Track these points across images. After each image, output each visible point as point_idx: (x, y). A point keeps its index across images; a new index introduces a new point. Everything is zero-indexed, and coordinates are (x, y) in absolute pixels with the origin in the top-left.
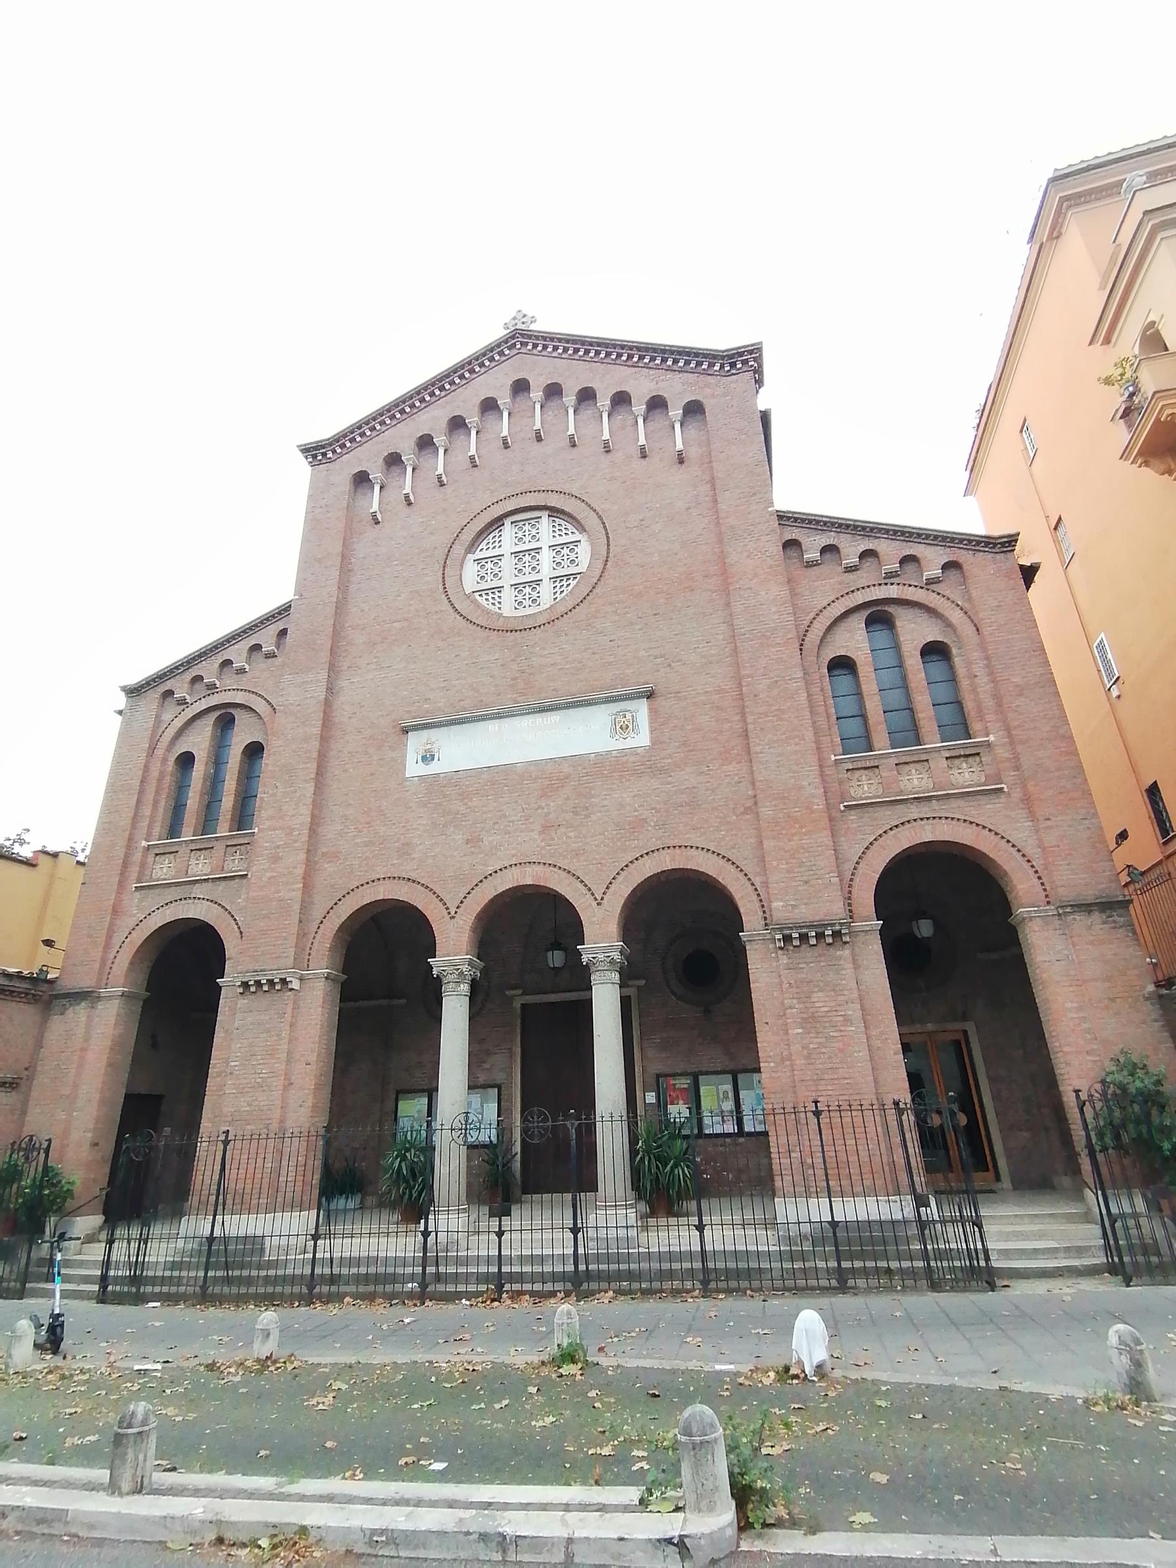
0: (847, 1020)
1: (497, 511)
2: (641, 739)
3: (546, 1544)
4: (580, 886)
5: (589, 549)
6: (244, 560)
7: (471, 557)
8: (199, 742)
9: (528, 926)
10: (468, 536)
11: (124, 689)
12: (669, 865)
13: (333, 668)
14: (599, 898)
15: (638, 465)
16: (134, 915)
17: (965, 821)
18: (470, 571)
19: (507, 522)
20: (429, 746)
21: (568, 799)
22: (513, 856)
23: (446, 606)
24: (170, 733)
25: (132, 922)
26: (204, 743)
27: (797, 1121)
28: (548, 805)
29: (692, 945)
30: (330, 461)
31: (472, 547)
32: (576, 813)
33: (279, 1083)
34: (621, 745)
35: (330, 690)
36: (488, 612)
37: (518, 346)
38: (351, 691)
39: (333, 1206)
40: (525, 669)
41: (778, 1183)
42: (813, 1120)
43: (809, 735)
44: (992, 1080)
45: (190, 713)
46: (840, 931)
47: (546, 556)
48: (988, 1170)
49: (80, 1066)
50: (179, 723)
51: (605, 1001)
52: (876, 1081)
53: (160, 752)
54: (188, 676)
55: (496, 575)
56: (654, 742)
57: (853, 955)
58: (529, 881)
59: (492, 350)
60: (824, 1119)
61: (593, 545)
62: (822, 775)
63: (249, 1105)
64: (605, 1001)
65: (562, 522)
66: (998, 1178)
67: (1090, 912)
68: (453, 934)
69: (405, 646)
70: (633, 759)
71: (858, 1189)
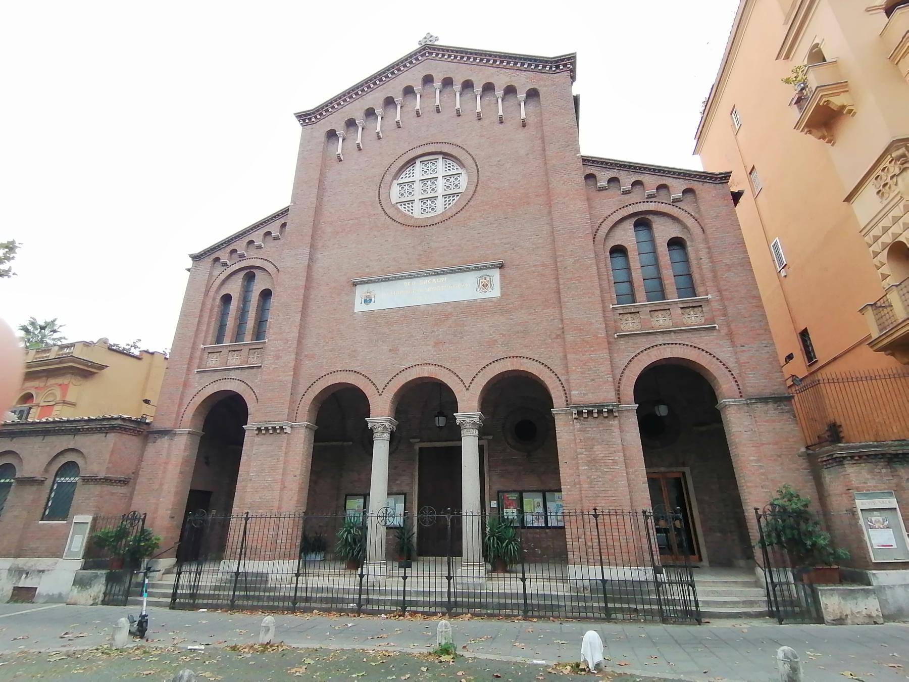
0: (615, 462)
6: (260, 181)
8: (234, 288)
9: (425, 401)
19: (418, 161)
25: (195, 391)
29: (522, 415)
31: (396, 176)
42: (593, 520)
45: (229, 271)
50: (222, 277)
51: (470, 446)
54: (229, 249)
56: (503, 294)
61: (469, 176)
63: (260, 498)
64: (470, 446)
66: (701, 559)
70: (490, 304)
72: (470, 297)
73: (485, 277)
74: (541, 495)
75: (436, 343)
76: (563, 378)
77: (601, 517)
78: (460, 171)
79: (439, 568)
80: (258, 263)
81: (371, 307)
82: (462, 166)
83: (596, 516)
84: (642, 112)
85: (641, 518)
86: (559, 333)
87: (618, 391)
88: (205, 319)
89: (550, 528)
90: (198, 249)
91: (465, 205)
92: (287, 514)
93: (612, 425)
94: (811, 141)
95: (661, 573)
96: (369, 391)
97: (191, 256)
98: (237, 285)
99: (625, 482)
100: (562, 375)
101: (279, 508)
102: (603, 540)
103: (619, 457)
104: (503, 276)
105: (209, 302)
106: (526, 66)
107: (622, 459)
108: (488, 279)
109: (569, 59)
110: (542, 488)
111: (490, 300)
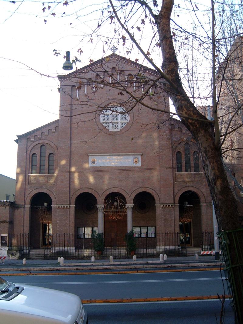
0: (172, 220)
2: (139, 164)
3: (183, 95)
6: (44, 108)
8: (37, 151)
9: (114, 198)
11: (17, 136)
12: (143, 191)
14: (130, 195)
17: (195, 187)
20: (94, 160)
22: (112, 186)
24: (30, 149)
25: (29, 192)
26: (36, 148)
30: (65, 81)
32: (125, 178)
34: (135, 165)
35: (71, 144)
40: (114, 143)
42: (64, 236)
44: (194, 229)
45: (34, 144)
46: (214, 164)
48: (190, 244)
50: (32, 146)
52: (175, 230)
53: (28, 153)
54: (33, 135)
55: (107, 119)
56: (141, 165)
60: (65, 236)
63: (62, 229)
64: (130, 214)
66: (191, 245)
67: (59, 269)
69: (87, 135)
71: (170, 245)
72: (131, 165)
73: (136, 158)
74: (147, 227)
75: (36, 165)
79: (71, 251)
81: (95, 165)
83: (166, 234)
85: (176, 234)
86: (159, 180)
88: (28, 164)
89: (141, 237)
93: (172, 210)
94: (55, 13)
97: (17, 136)
99: (174, 225)
100: (159, 194)
102: (65, 242)
104: (142, 159)
105: (28, 156)
106: (132, 65)
108: (137, 159)
110: (147, 225)
111: (137, 167)
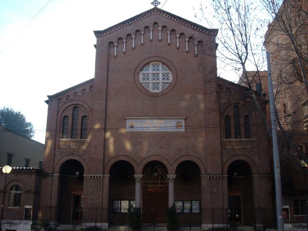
1: (149, 60)
4: (167, 162)
5: (172, 76)
6: (81, 68)
7: (141, 72)
8: (69, 113)
9: (154, 167)
10: (140, 67)
13: (106, 100)
15: (185, 54)
16: (59, 157)
18: (141, 76)
19: (151, 63)
20: (132, 124)
21: (165, 142)
23: (135, 86)
24: (62, 110)
27: (92, 210)
28: (161, 142)
29: (188, 172)
31: (141, 70)
33: (101, 198)
34: (178, 130)
36: (145, 89)
37: (156, 12)
38: (111, 106)
39: (77, 226)
40: (155, 105)
41: (203, 221)
42: (95, 210)
43: (219, 134)
45: (66, 105)
47: (161, 76)
49: (52, 191)
50: (64, 108)
51: (171, 186)
55: (148, 79)
57: (222, 181)
58: (156, 160)
59: (148, 12)
61: (172, 73)
62: (221, 143)
64: (171, 186)
65: (165, 67)
66: (241, 223)
68: (139, 170)
70: (181, 134)
76: (205, 164)
77: (98, 209)
78: (169, 72)
80: (80, 103)
82: (170, 70)
83: (96, 209)
84: (242, 54)
87: (222, 170)
90: (52, 94)
91: (170, 89)
92: (216, 208)
95: (228, 224)
96: (134, 164)
98: (65, 108)
101: (102, 205)
103: (221, 192)
105: (59, 119)
107: (221, 192)
109: (215, 31)
111: (181, 132)
